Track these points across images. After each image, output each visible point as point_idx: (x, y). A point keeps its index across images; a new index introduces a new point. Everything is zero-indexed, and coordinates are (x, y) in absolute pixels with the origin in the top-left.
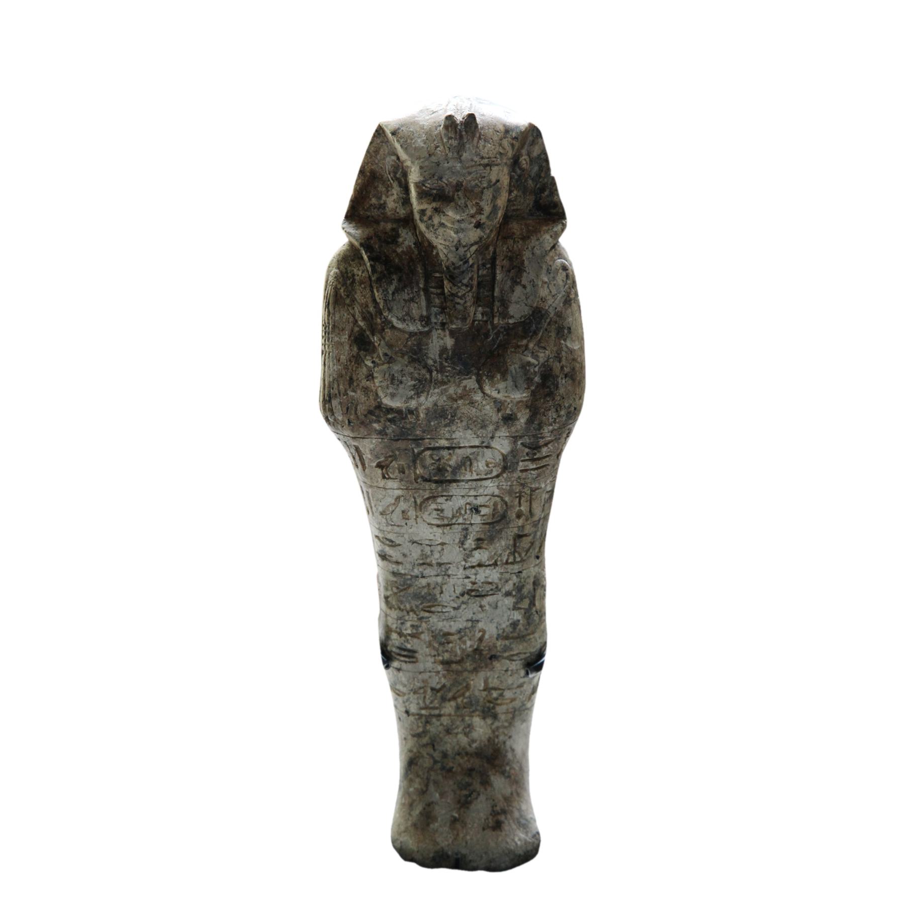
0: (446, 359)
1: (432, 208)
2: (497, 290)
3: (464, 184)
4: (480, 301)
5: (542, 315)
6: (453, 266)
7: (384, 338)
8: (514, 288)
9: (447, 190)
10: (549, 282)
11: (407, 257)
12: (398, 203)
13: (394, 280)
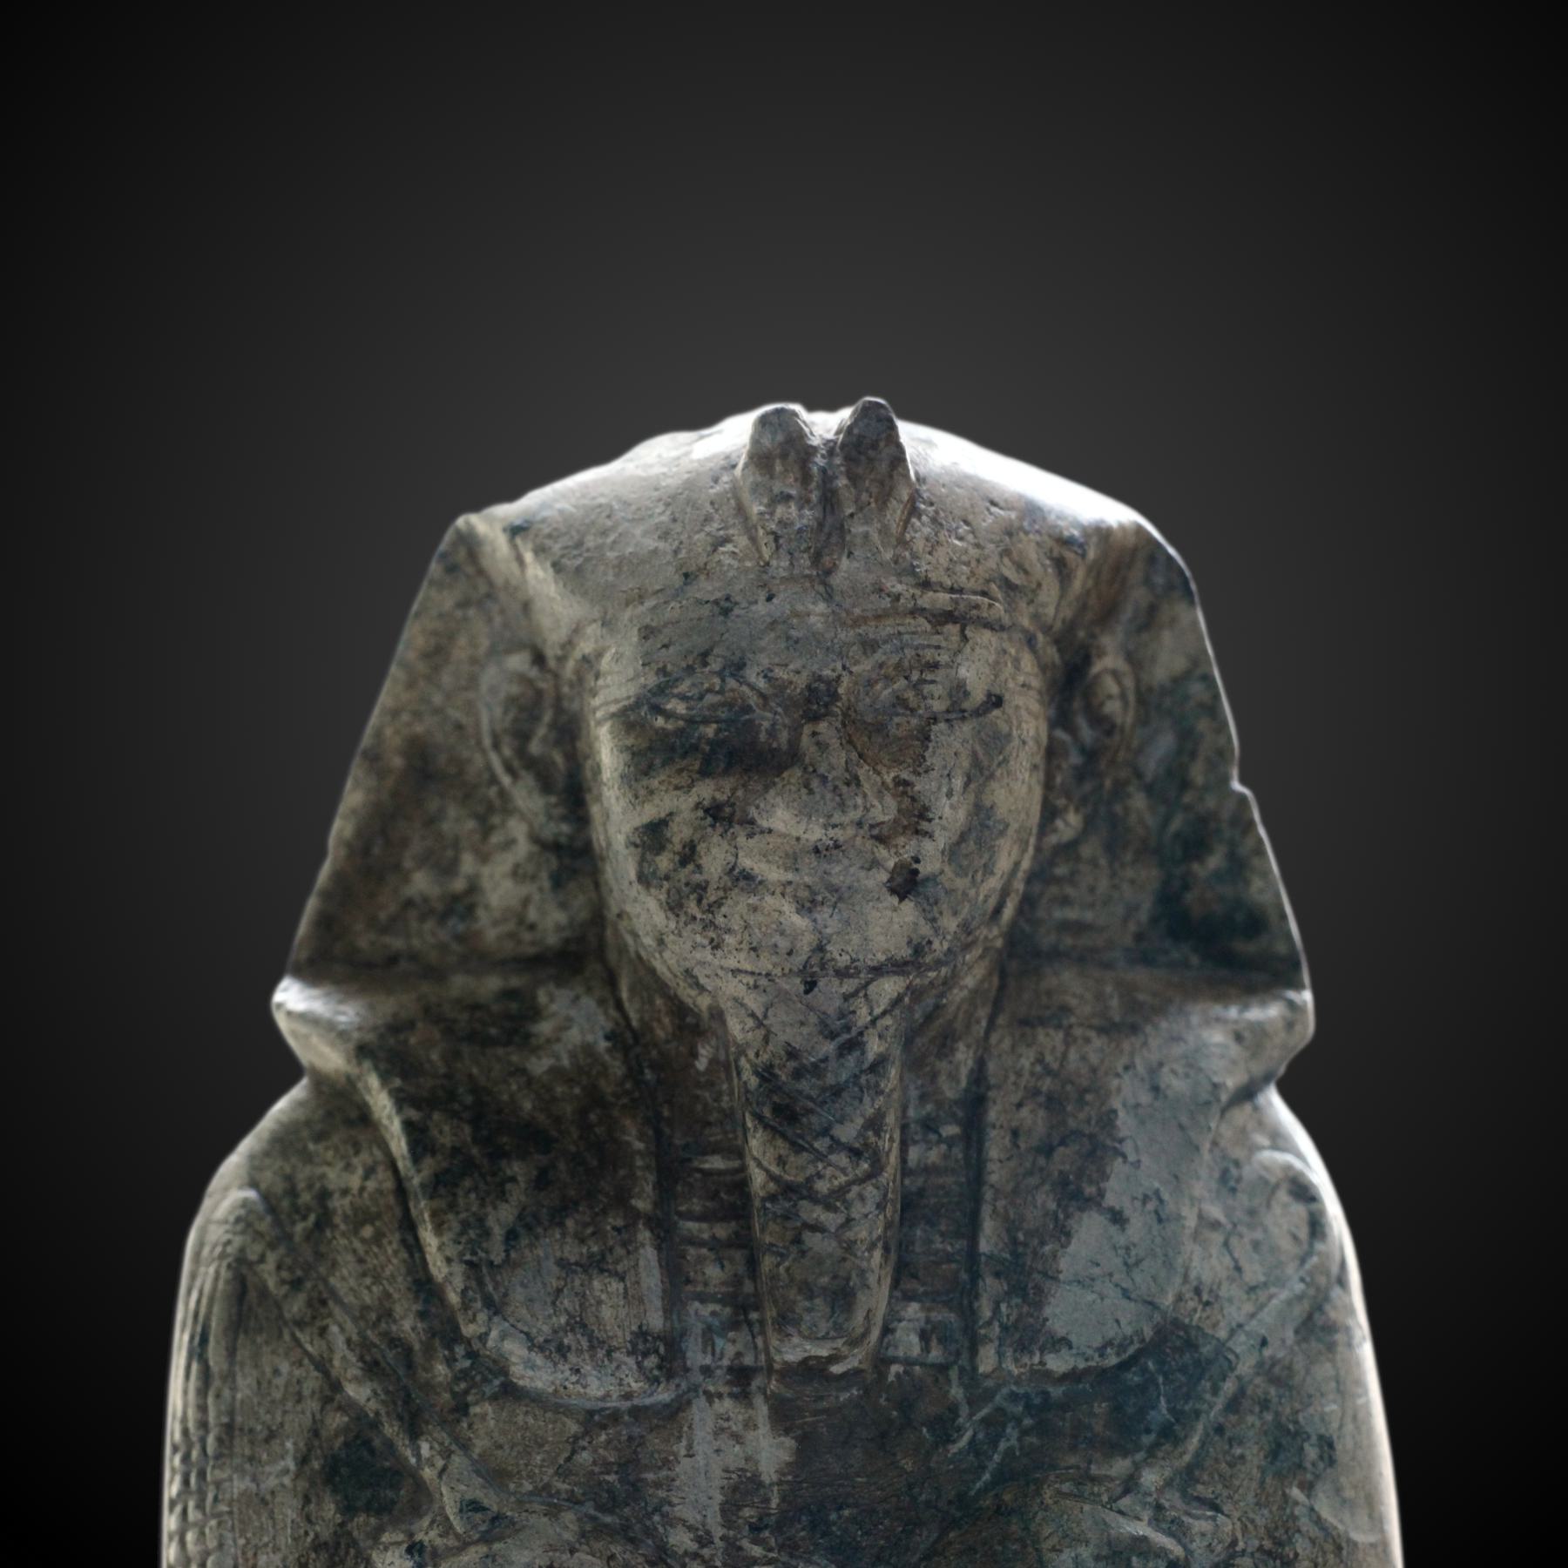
0: (755, 1529)
1: (698, 806)
2: (989, 1226)
3: (841, 691)
4: (914, 1276)
5: (1198, 1363)
6: (792, 1064)
7: (465, 1447)
8: (1071, 1222)
9: (766, 724)
10: (1229, 1227)
11: (577, 1091)
12: (533, 878)
13: (513, 1179)
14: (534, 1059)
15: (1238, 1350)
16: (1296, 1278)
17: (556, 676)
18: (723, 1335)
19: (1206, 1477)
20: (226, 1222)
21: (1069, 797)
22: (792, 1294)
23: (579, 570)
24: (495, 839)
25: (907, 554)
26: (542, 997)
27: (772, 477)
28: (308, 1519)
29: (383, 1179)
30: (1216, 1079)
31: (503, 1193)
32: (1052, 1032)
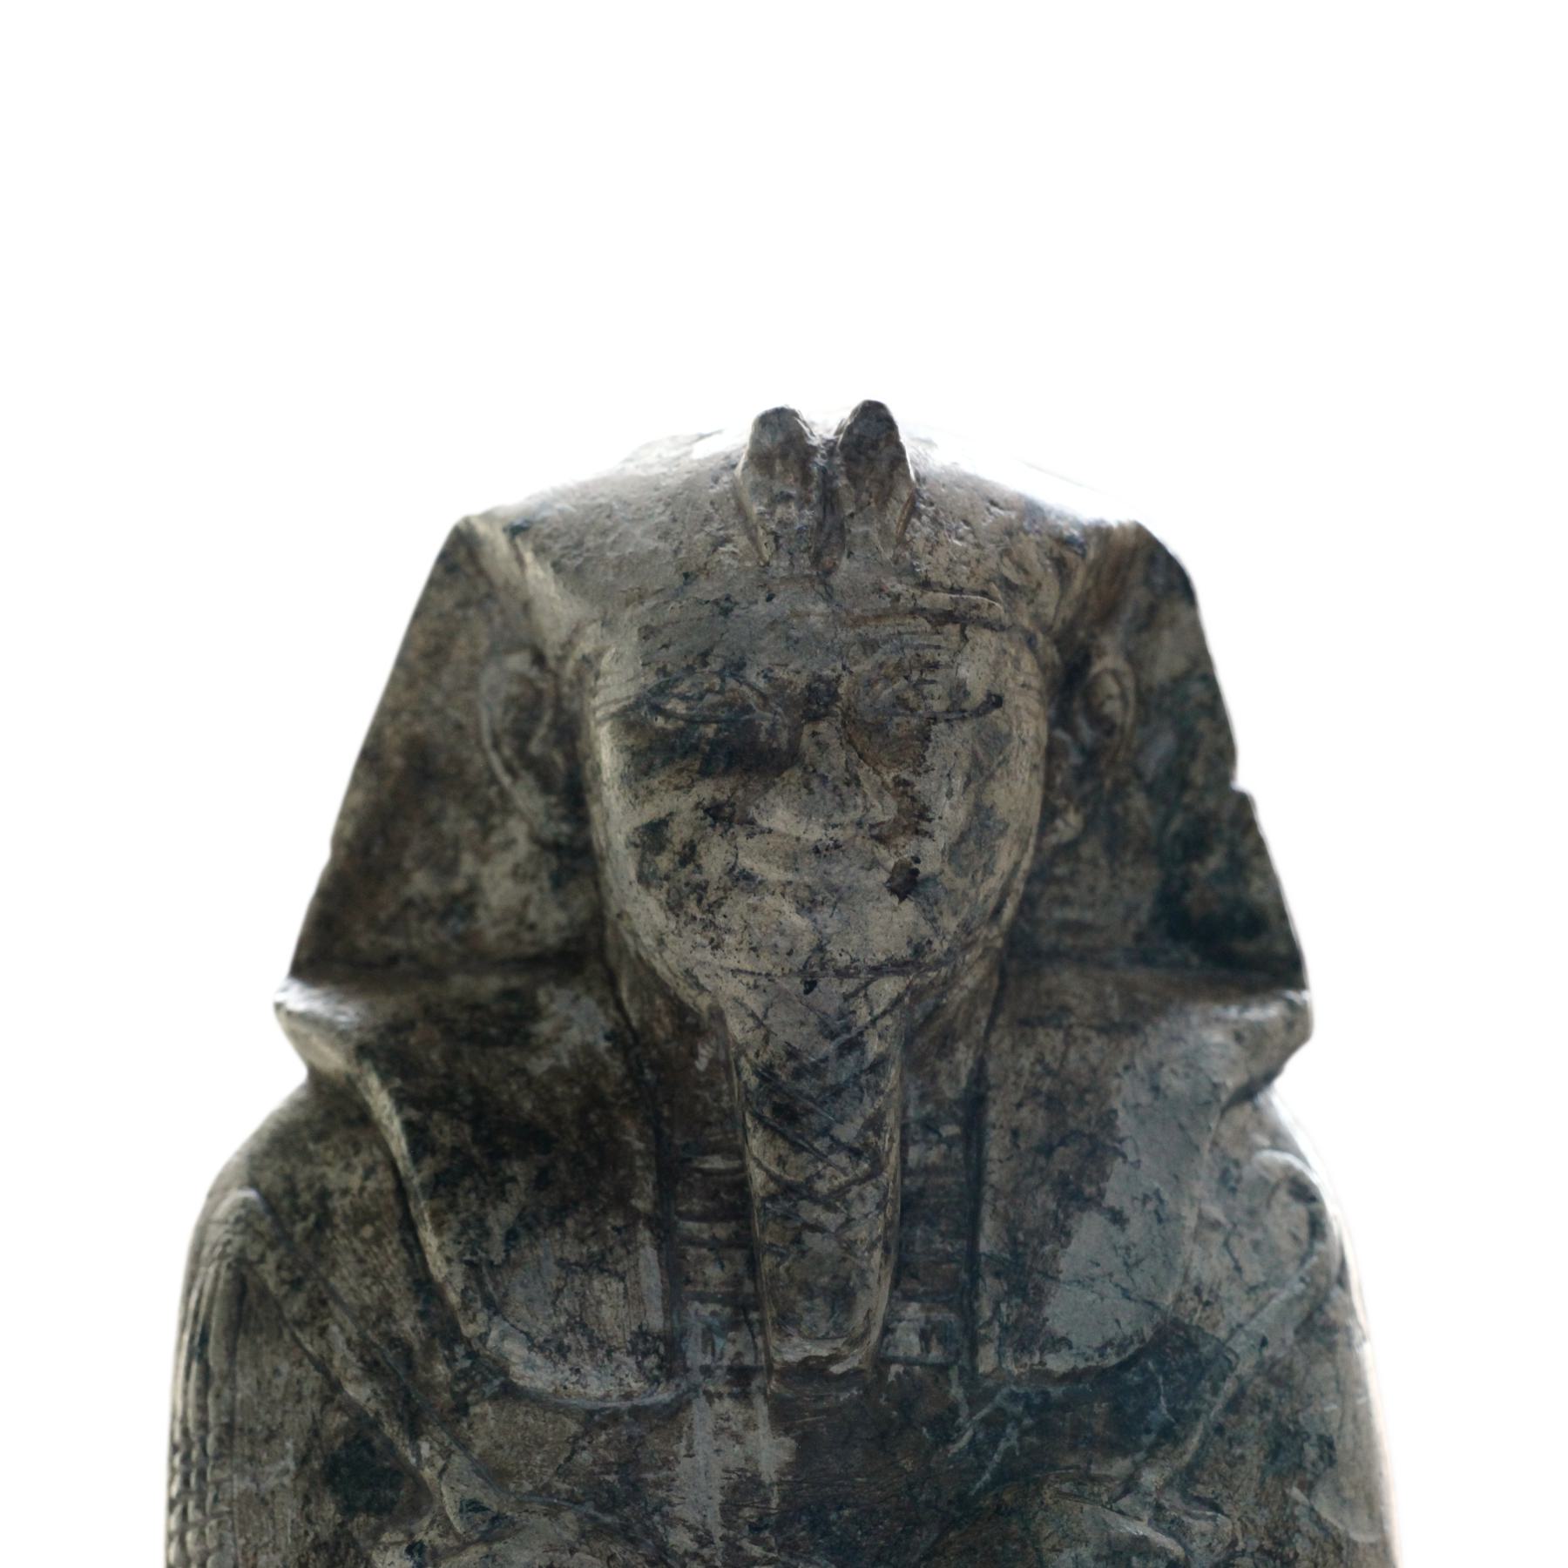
0: (755, 1529)
1: (698, 806)
2: (989, 1226)
3: (841, 691)
4: (914, 1276)
5: (1198, 1363)
6: (792, 1064)
7: (465, 1447)
8: (1071, 1222)
9: (766, 724)
10: (1229, 1227)
11: (577, 1091)
12: (533, 878)
13: (513, 1179)
14: (534, 1059)
15: (1238, 1350)
16: (1296, 1278)
17: (556, 676)
18: (723, 1335)
19: (1206, 1477)
20: (226, 1222)
21: (1069, 797)
22: (792, 1294)
23: (579, 570)
24: (495, 839)
25: (907, 554)
26: (542, 997)
27: (772, 477)
28: (308, 1519)
29: (383, 1179)
30: (1216, 1079)
31: (503, 1193)
32: (1052, 1032)
